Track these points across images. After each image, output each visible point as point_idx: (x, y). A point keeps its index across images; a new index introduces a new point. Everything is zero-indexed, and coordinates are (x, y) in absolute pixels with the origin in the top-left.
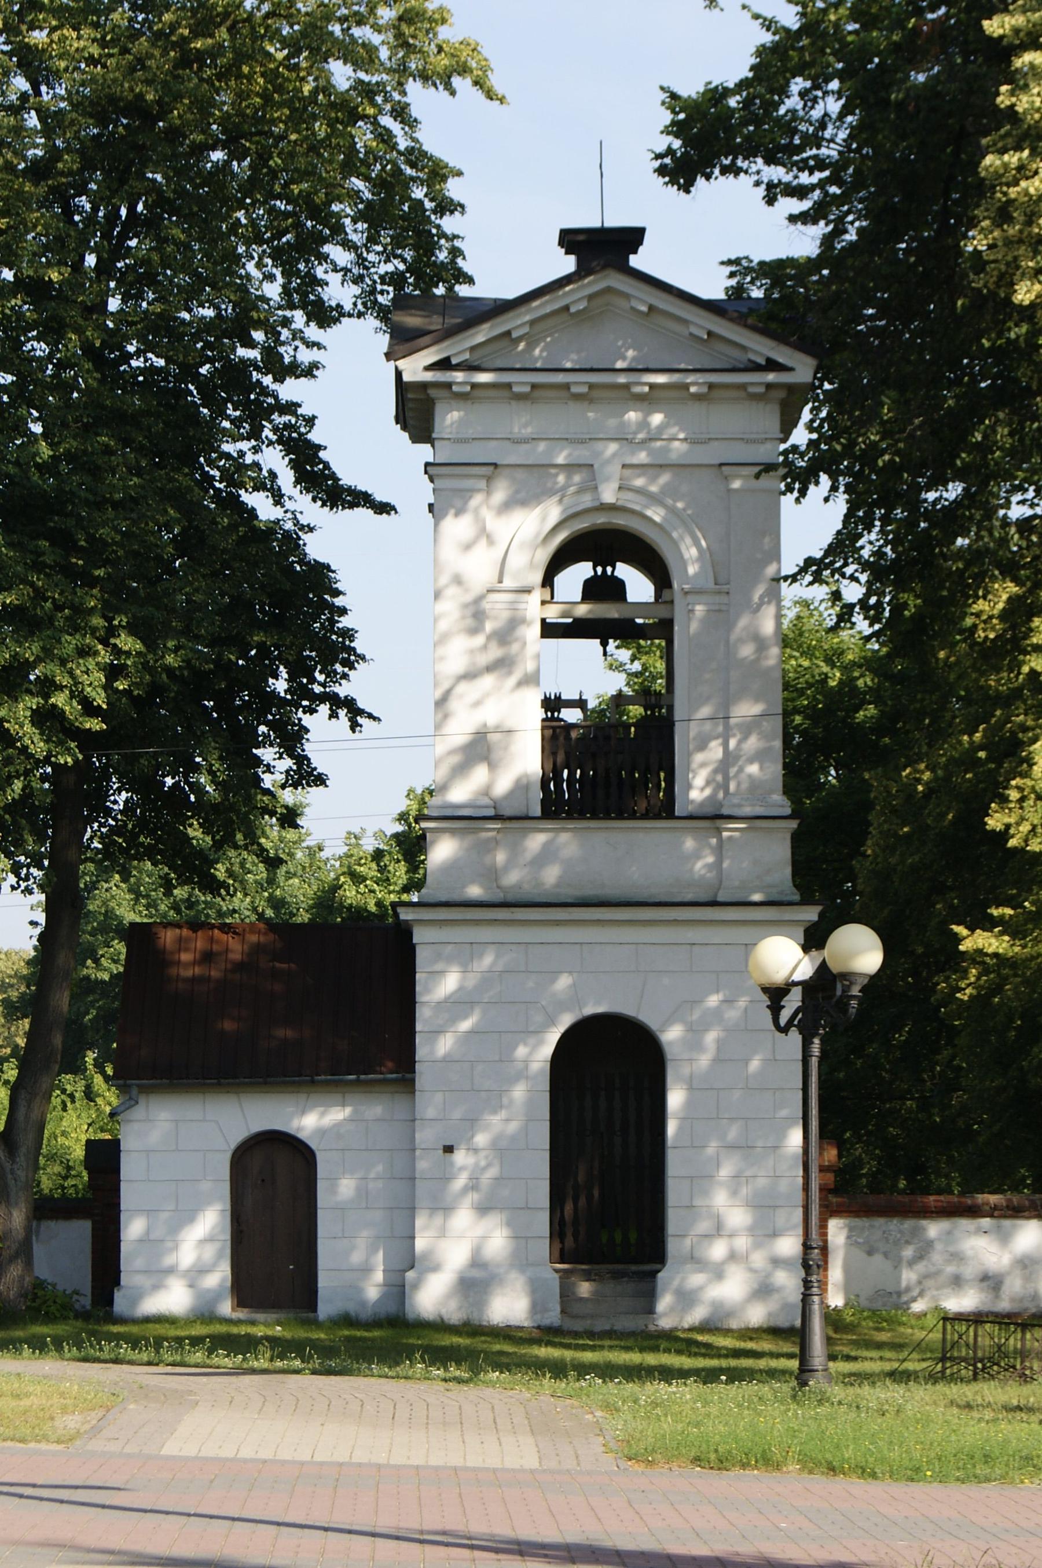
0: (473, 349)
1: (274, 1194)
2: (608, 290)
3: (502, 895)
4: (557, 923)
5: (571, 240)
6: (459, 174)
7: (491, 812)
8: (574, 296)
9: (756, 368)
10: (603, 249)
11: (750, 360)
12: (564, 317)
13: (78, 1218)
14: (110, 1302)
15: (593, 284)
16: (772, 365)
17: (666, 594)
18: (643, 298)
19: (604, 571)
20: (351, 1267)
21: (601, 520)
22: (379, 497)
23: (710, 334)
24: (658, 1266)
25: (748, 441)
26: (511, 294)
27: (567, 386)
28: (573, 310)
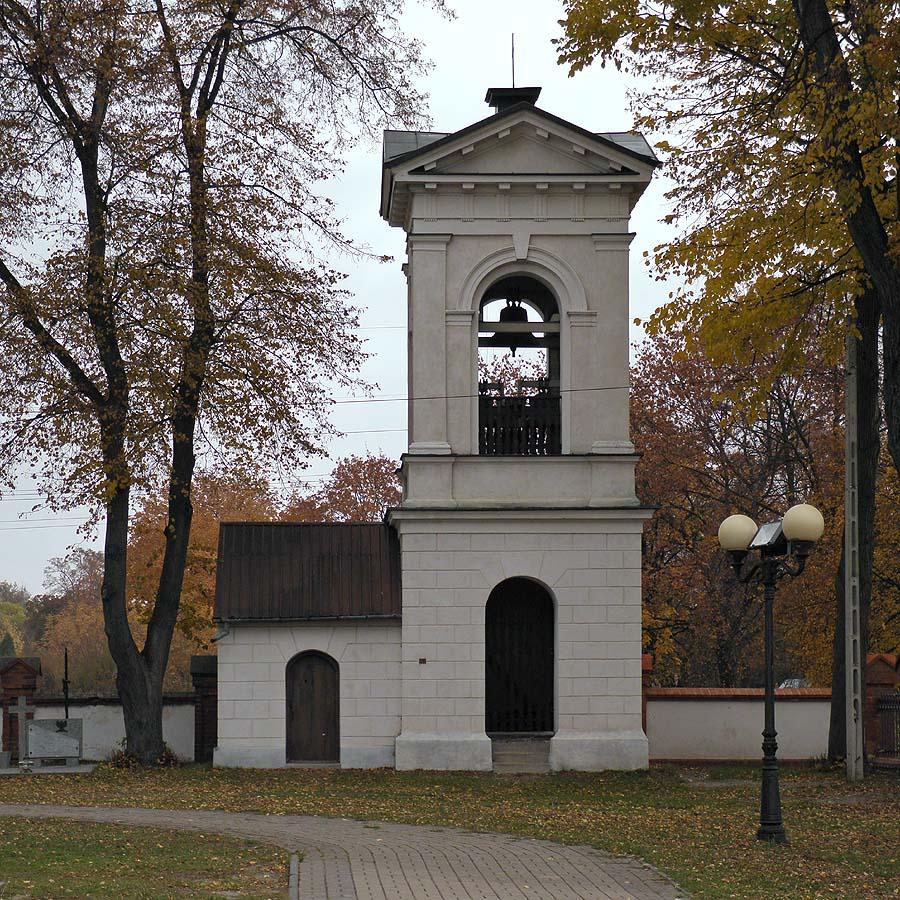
0: (438, 161)
1: (313, 688)
5: (495, 96)
7: (449, 452)
8: (503, 129)
9: (616, 173)
10: (513, 101)
11: (611, 168)
13: (187, 704)
14: (210, 757)
15: (514, 121)
16: (625, 171)
17: (554, 317)
18: (544, 129)
19: (514, 304)
20: (361, 737)
21: (515, 269)
24: (552, 733)
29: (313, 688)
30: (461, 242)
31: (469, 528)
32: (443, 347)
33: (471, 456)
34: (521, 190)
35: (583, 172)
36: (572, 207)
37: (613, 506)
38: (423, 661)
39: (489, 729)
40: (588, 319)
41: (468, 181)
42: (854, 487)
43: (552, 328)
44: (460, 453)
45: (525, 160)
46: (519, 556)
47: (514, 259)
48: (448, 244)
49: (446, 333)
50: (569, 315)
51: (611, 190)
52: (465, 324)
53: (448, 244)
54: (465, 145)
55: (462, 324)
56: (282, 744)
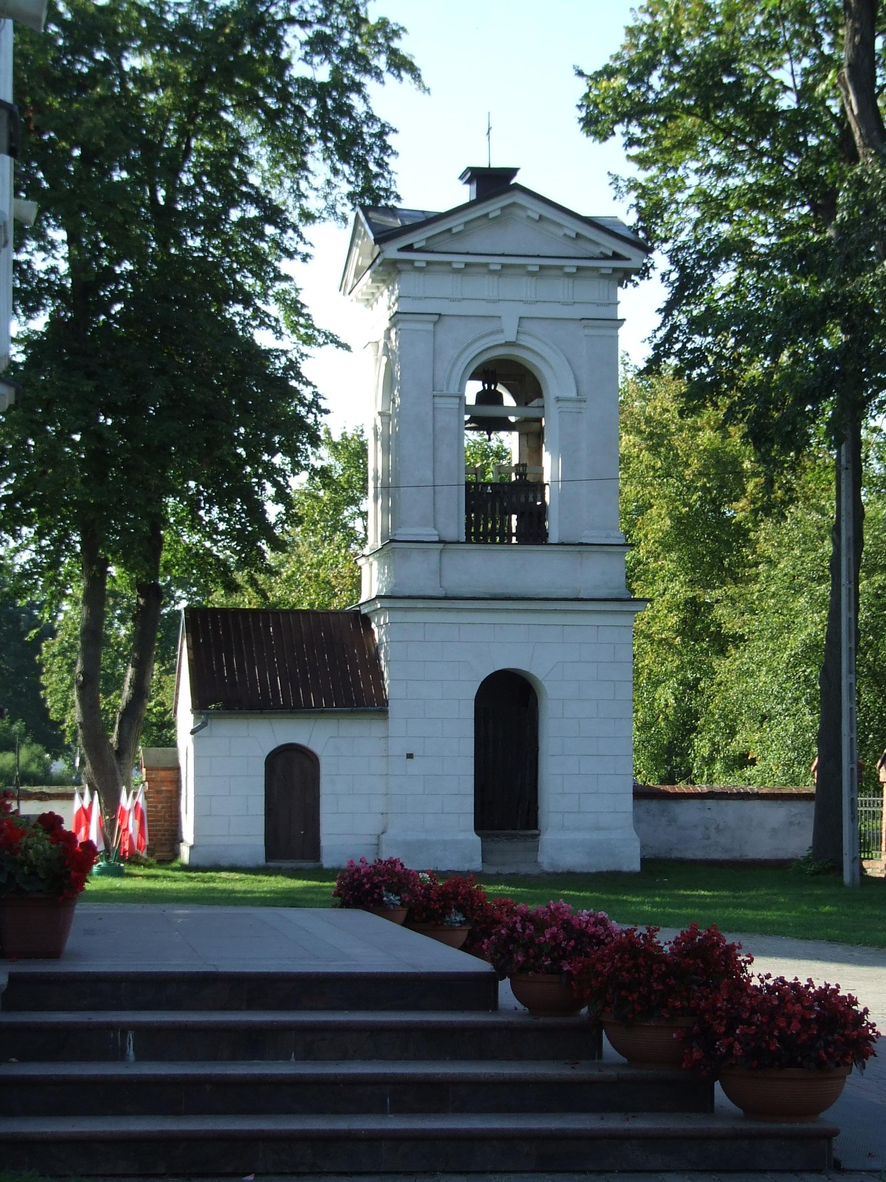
0: (428, 239)
1: (292, 782)
2: (513, 204)
3: (444, 592)
4: (448, 610)
6: (395, 131)
7: (437, 539)
9: (606, 257)
12: (447, 235)
16: (616, 256)
22: (342, 340)
23: (577, 234)
24: (536, 832)
25: (598, 305)
26: (443, 209)
27: (486, 265)
28: (491, 216)
29: (292, 782)
30: (447, 318)
31: (608, 553)
32: (431, 431)
33: (458, 542)
34: (509, 268)
35: (572, 255)
36: (561, 289)
37: (604, 597)
38: (410, 756)
39: (479, 827)
40: (578, 405)
41: (459, 261)
42: (850, 583)
43: (530, 412)
44: (448, 539)
45: (514, 238)
46: (506, 644)
47: (503, 341)
48: (435, 323)
49: (434, 416)
50: (558, 399)
51: (601, 274)
52: (451, 406)
53: (435, 323)
54: (456, 224)
55: (449, 406)
56: (260, 841)
